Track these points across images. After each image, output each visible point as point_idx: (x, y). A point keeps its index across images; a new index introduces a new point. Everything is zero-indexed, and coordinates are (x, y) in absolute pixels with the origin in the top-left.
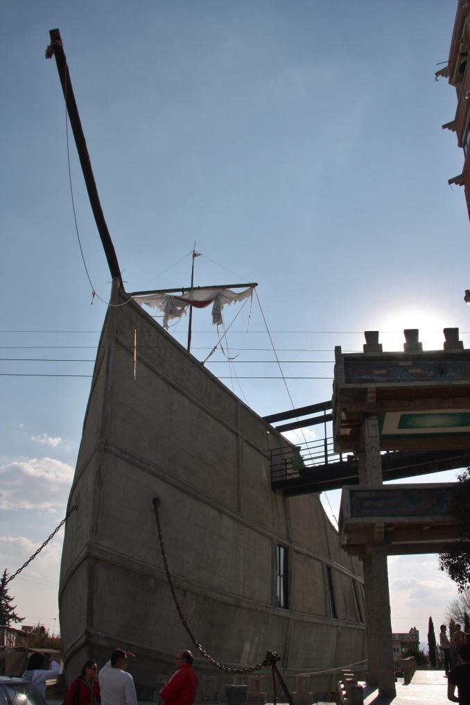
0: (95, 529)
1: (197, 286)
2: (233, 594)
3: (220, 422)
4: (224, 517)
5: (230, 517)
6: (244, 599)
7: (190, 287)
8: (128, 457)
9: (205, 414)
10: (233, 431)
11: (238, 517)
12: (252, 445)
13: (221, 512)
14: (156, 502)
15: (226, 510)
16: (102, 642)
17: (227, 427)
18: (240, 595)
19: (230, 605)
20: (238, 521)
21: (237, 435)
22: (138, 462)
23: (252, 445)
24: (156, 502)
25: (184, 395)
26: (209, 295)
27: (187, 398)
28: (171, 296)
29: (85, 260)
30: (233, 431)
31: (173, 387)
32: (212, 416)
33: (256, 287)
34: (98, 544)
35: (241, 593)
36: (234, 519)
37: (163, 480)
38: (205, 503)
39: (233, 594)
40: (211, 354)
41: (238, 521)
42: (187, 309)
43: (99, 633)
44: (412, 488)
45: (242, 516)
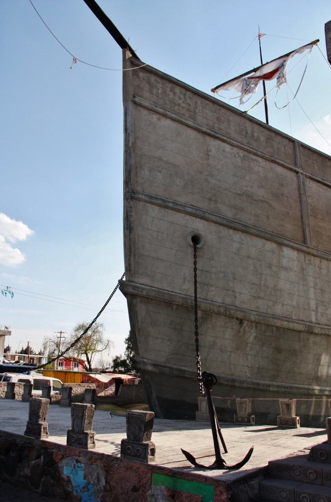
0: (128, 269)
1: (266, 63)
2: (302, 321)
3: (273, 162)
4: (285, 249)
5: (293, 248)
6: (317, 325)
7: (261, 65)
8: (159, 202)
9: (252, 156)
10: (291, 169)
11: (304, 249)
12: (318, 181)
13: (280, 244)
14: (196, 239)
15: (286, 242)
16: (150, 368)
17: (283, 166)
18: (312, 322)
19: (300, 332)
20: (303, 251)
21: (297, 173)
22: (171, 205)
23: (318, 181)
24: (196, 239)
25: (224, 141)
26: (275, 65)
27: (228, 144)
28: (245, 79)
29: (33, 4)
30: (291, 169)
31: (209, 135)
32: (263, 157)
33: (318, 43)
34: (132, 282)
35: (314, 320)
36: (298, 250)
37: (202, 218)
38: (257, 236)
39: (302, 321)
40: (257, 103)
41: (303, 251)
42: (261, 81)
43: (145, 360)
44: (260, 123)
45: (308, 247)
